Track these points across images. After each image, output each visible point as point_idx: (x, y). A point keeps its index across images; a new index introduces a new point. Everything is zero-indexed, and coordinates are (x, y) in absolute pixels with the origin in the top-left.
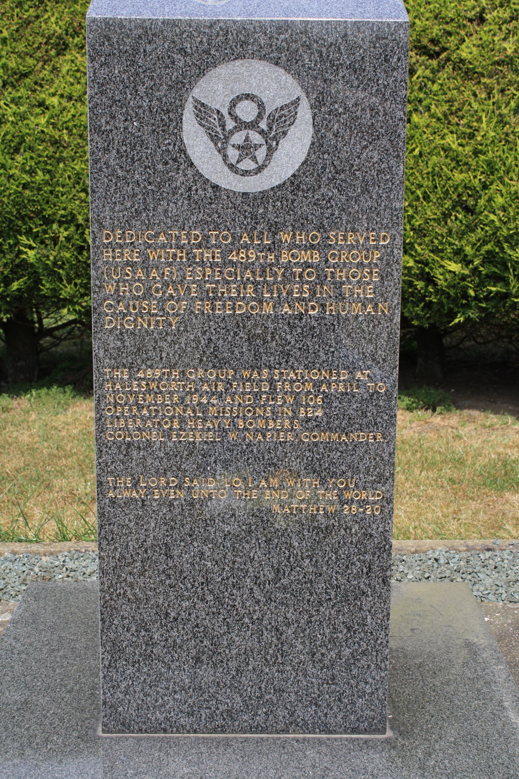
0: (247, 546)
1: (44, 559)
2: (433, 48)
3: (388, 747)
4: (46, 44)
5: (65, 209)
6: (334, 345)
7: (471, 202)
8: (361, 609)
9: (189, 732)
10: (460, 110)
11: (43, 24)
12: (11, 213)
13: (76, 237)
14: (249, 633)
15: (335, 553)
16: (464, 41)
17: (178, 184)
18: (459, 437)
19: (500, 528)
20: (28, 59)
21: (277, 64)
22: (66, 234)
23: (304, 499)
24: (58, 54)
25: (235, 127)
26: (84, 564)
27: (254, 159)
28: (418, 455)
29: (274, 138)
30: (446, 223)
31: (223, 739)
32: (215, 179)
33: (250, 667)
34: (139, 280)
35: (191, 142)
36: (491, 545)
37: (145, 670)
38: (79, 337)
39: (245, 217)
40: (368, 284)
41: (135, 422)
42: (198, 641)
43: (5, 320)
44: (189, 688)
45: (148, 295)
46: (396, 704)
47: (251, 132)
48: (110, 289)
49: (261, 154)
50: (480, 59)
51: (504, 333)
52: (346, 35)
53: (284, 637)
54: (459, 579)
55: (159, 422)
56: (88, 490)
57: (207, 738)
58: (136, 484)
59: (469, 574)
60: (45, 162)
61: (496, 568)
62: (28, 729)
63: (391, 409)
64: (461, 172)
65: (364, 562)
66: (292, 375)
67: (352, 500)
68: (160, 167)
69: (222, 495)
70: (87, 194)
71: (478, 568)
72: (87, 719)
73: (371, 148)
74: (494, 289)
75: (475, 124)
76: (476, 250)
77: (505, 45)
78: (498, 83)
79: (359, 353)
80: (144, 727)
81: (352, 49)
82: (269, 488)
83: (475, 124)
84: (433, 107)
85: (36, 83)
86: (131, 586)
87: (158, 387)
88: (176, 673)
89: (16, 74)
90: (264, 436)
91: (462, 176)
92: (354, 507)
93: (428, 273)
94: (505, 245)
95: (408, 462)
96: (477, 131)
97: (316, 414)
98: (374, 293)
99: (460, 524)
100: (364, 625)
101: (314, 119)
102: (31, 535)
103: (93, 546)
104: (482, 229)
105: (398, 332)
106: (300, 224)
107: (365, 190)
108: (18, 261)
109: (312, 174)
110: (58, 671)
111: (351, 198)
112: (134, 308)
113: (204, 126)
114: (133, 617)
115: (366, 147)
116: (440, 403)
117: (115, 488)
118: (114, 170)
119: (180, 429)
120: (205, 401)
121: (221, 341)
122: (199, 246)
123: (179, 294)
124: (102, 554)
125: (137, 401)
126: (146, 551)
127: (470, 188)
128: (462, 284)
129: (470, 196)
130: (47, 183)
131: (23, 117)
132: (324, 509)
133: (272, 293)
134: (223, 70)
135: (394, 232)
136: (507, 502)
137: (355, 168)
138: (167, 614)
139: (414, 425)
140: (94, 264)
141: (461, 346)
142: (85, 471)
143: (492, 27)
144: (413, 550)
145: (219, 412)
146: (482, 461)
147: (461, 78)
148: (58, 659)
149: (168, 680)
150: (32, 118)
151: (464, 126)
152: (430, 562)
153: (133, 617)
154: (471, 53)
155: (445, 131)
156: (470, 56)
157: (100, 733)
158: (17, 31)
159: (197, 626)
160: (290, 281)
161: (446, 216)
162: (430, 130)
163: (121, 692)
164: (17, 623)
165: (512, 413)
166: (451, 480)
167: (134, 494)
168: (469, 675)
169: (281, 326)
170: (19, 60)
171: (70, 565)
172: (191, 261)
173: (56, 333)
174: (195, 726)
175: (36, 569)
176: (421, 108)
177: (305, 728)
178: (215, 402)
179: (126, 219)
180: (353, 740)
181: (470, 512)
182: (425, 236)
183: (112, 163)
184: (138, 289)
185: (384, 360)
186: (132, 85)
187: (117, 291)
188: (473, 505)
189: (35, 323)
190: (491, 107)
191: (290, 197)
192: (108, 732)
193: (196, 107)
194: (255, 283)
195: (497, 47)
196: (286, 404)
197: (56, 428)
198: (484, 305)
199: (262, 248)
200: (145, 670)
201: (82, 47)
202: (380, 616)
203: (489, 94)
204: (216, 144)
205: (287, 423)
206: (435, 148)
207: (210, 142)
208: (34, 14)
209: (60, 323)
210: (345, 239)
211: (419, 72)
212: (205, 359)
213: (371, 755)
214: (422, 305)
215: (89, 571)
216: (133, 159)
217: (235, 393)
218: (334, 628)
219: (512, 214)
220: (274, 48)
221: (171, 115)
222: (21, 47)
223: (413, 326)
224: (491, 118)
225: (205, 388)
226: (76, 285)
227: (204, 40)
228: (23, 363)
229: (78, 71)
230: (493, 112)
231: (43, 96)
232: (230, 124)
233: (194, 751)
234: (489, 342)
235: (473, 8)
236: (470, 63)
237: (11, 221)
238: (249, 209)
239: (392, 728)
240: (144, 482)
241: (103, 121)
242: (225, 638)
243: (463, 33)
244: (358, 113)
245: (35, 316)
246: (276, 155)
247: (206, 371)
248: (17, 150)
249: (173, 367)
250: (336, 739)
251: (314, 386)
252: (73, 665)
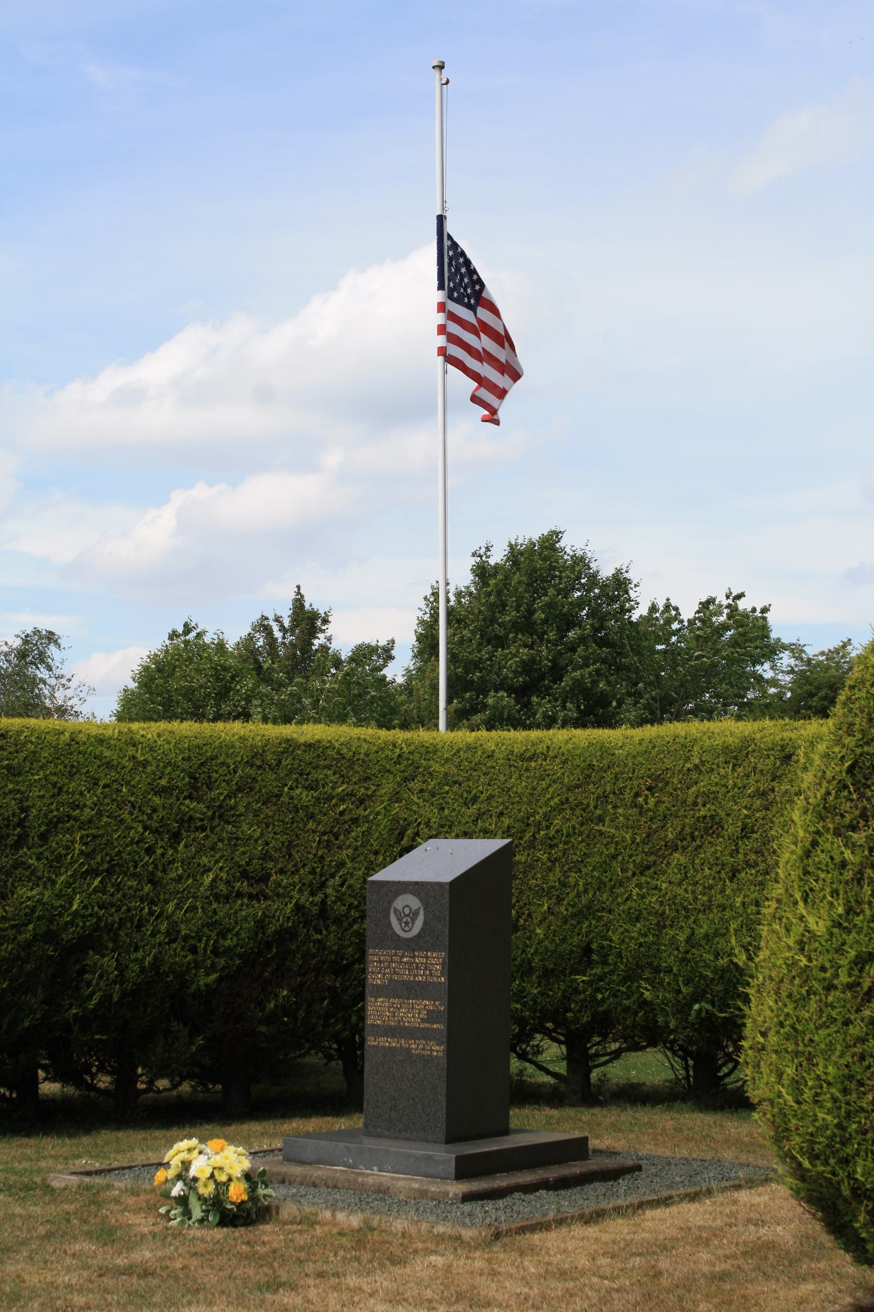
134: (401, 897)
248: (637, 919)
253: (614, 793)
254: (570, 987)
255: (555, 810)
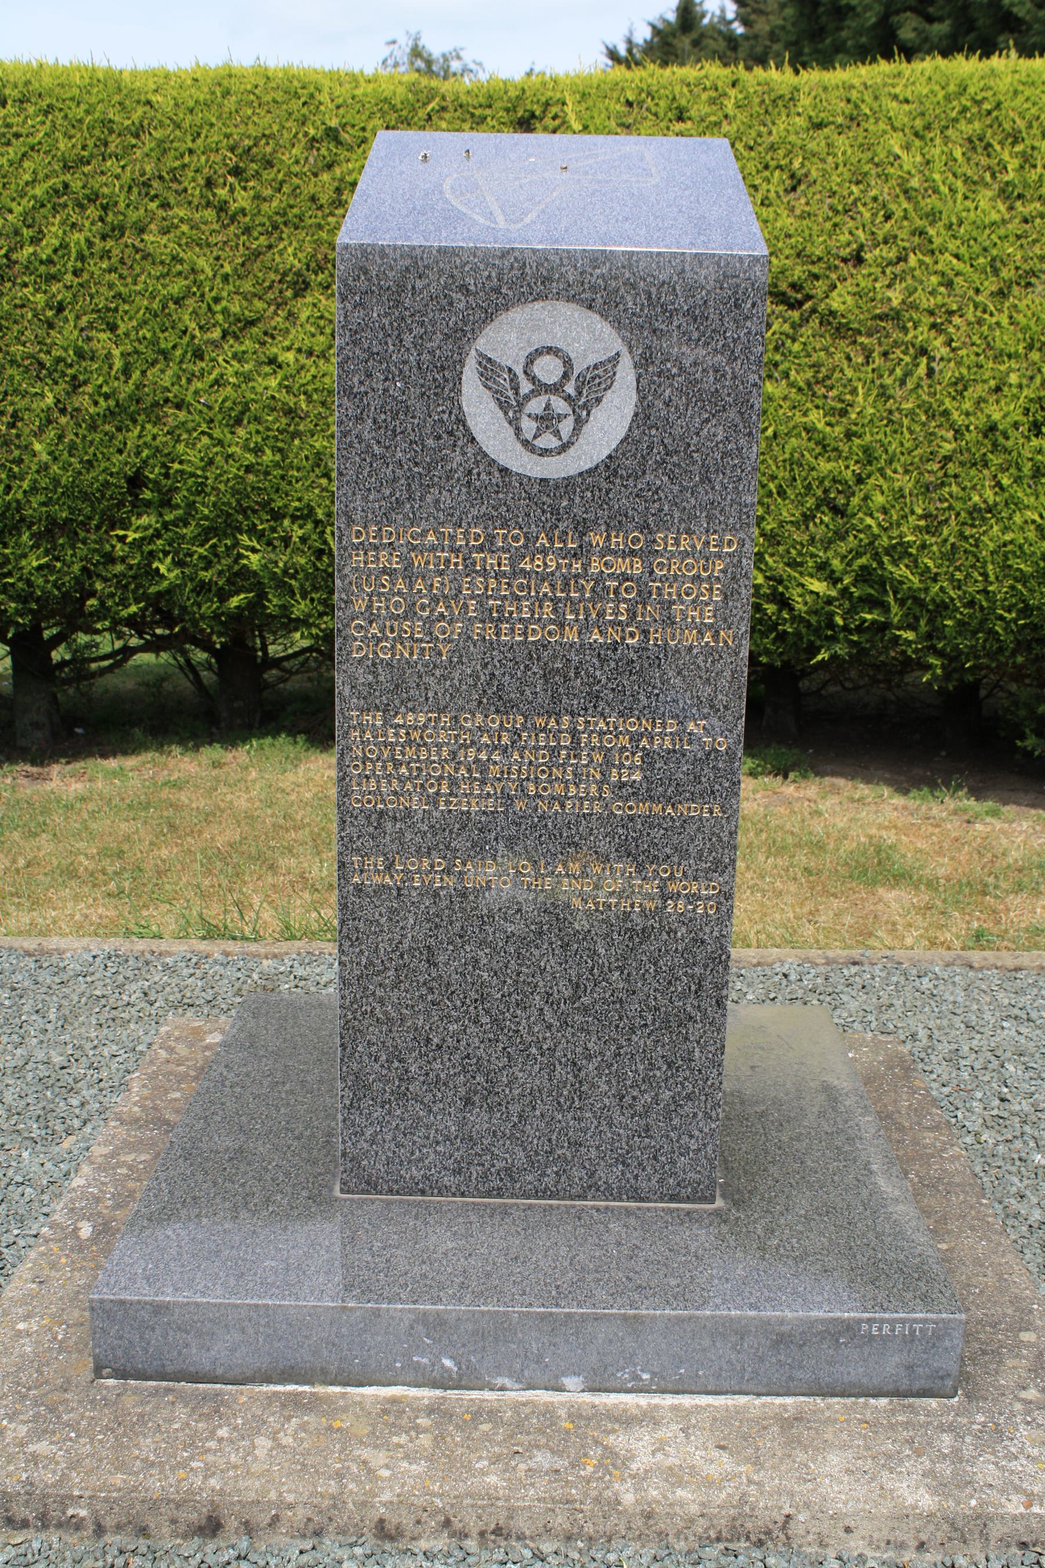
0: (536, 952)
1: (265, 962)
2: (794, 295)
3: (717, 1220)
4: (280, 282)
5: (300, 500)
6: (659, 685)
7: (841, 501)
8: (686, 1039)
9: (454, 1195)
10: (828, 377)
11: (277, 256)
12: (229, 504)
13: (314, 537)
14: (537, 1067)
15: (655, 964)
16: (835, 287)
17: (455, 466)
18: (818, 813)
19: (870, 935)
20: (256, 301)
21: (590, 307)
22: (300, 533)
23: (614, 892)
24: (296, 295)
25: (533, 391)
26: (318, 970)
27: (557, 433)
28: (764, 836)
29: (585, 406)
30: (807, 528)
31: (500, 1205)
32: (503, 460)
33: (538, 1113)
34: (399, 593)
35: (472, 410)
36: (857, 958)
37: (398, 1112)
38: (316, 669)
39: (544, 512)
40: (707, 604)
41: (390, 783)
42: (468, 1076)
43: (218, 646)
44: (456, 1137)
45: (410, 613)
46: (730, 1165)
47: (553, 398)
48: (360, 605)
49: (566, 427)
50: (857, 311)
51: (880, 677)
52: (683, 271)
53: (582, 1074)
54: (815, 1002)
55: (422, 785)
56: (325, 873)
57: (479, 1204)
58: (389, 867)
59: (830, 997)
60: (276, 438)
61: (864, 987)
62: (243, 1185)
63: (734, 774)
64: (829, 460)
65: (692, 976)
66: (602, 725)
67: (679, 894)
68: (430, 442)
69: (505, 883)
70: (330, 480)
71: (840, 988)
72: (320, 1174)
73: (714, 422)
74: (869, 617)
75: (848, 397)
76: (848, 565)
77: (890, 294)
78: (880, 344)
79: (692, 697)
80: (396, 1187)
81: (690, 290)
82: (568, 875)
83: (848, 397)
84: (793, 373)
85: (266, 333)
86: (382, 1002)
87: (422, 738)
88: (439, 1117)
89: (239, 321)
90: (563, 806)
91: (829, 466)
92: (681, 904)
93: (782, 594)
94: (886, 559)
95: (750, 845)
96: (851, 406)
97: (633, 778)
98: (715, 616)
99: (818, 929)
100: (690, 1060)
101: (638, 382)
102: (248, 931)
103: (332, 948)
104: (855, 537)
105: (746, 669)
106: (617, 522)
107: (706, 479)
108: (236, 568)
109: (634, 455)
110: (283, 1111)
111: (686, 489)
112: (392, 631)
113: (490, 389)
114: (383, 1043)
115: (707, 421)
116: (793, 767)
117: (362, 871)
118: (369, 446)
119: (450, 795)
120: (485, 758)
121: (507, 677)
122: (481, 549)
123: (452, 614)
124: (343, 958)
125: (393, 755)
126: (402, 956)
127: (840, 482)
128: (827, 608)
129: (839, 492)
130: (277, 465)
131: (247, 378)
132: (641, 905)
133: (577, 614)
134: (518, 315)
135: (742, 535)
136: (880, 900)
137: (693, 448)
138: (428, 1040)
139: (758, 796)
140: (339, 571)
141: (823, 692)
142: (321, 847)
143: (872, 270)
144: (755, 961)
145: (503, 772)
146: (848, 846)
147: (831, 335)
148: (283, 1095)
149: (428, 1127)
150: (260, 380)
151: (833, 399)
152: (776, 979)
153: (383, 1043)
154: (844, 303)
155: (809, 405)
156: (843, 307)
157: (337, 1193)
158: (243, 265)
159: (468, 1057)
160: (601, 598)
161: (808, 518)
162: (788, 403)
163: (366, 1141)
164: (230, 1046)
165: (889, 783)
166: (807, 870)
167: (388, 880)
168: (826, 1128)
169: (588, 658)
170: (245, 303)
171: (300, 972)
172: (470, 568)
173: (286, 664)
174: (463, 1188)
175: (255, 976)
176: (776, 375)
177: (609, 1193)
178: (498, 759)
179: (383, 510)
180: (671, 1211)
181: (831, 913)
182: (779, 543)
183: (366, 435)
184: (397, 605)
185: (726, 707)
186: (396, 333)
187: (370, 607)
188: (836, 903)
189: (256, 651)
190: (870, 376)
191: (605, 485)
192: (348, 1192)
193: (480, 363)
194: (555, 601)
195: (879, 296)
196: (592, 763)
197: (283, 791)
198: (855, 638)
199: (564, 553)
200: (398, 1112)
201: (328, 287)
202: (712, 1049)
203: (867, 358)
204: (506, 413)
205: (593, 788)
206: (794, 427)
207: (498, 409)
208: (266, 243)
209: (290, 651)
210: (677, 543)
211: (775, 327)
212: (485, 700)
213: (695, 1231)
214: (774, 635)
215: (324, 980)
216: (394, 431)
217: (524, 748)
218: (650, 1064)
219: (895, 517)
220: (586, 286)
221: (446, 373)
222: (247, 286)
223: (760, 663)
224: (869, 390)
225: (485, 739)
226: (312, 600)
227: (494, 274)
228: (241, 703)
229: (322, 317)
230: (873, 382)
231: (275, 350)
232: (526, 387)
233: (461, 1220)
234: (860, 687)
235: (848, 244)
236: (843, 316)
237: (229, 515)
238: (549, 501)
239: (723, 1196)
240: (400, 864)
241: (356, 380)
242: (505, 1073)
243: (834, 276)
244: (698, 376)
245: (258, 641)
246: (586, 429)
247: (486, 716)
248: (238, 422)
249: (442, 711)
250: (648, 1209)
251: (631, 740)
252: (303, 1103)
253: (161, 177)
254: (95, 550)
255: (43, 206)
